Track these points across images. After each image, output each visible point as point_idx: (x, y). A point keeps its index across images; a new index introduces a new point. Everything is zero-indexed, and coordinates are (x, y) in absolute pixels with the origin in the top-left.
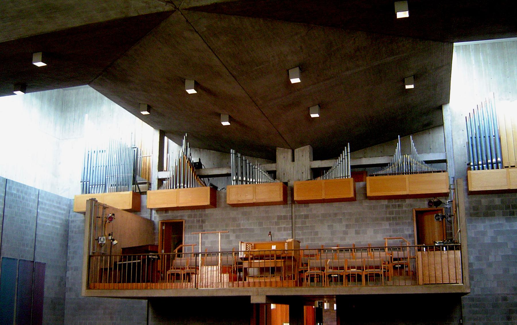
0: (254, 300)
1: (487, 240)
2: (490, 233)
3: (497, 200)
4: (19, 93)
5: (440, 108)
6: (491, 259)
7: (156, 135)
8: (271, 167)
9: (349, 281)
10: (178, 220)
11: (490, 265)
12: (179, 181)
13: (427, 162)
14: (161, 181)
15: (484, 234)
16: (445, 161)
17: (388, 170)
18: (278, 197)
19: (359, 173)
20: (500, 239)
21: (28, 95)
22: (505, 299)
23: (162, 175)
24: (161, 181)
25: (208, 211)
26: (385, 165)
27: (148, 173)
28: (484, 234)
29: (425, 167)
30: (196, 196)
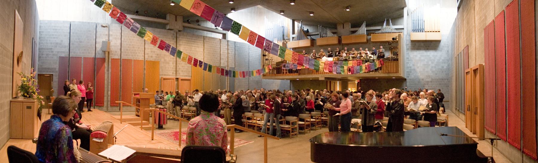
0: (320, 79)
1: (417, 58)
2: (419, 56)
3: (422, 44)
4: (233, 11)
5: (403, 8)
6: (419, 65)
7: (290, 21)
8: (334, 31)
9: (234, 72)
10: (409, 43)
11: (418, 67)
12: (299, 38)
13: (396, 29)
14: (293, 38)
15: (416, 56)
16: (403, 29)
17: (380, 32)
18: (336, 42)
19: (369, 33)
20: (422, 58)
21: (236, 12)
22: (423, 80)
23: (294, 36)
24: (293, 38)
25: (311, 48)
26: (379, 30)
27: (288, 36)
28: (416, 56)
29: (396, 31)
30: (305, 43)
